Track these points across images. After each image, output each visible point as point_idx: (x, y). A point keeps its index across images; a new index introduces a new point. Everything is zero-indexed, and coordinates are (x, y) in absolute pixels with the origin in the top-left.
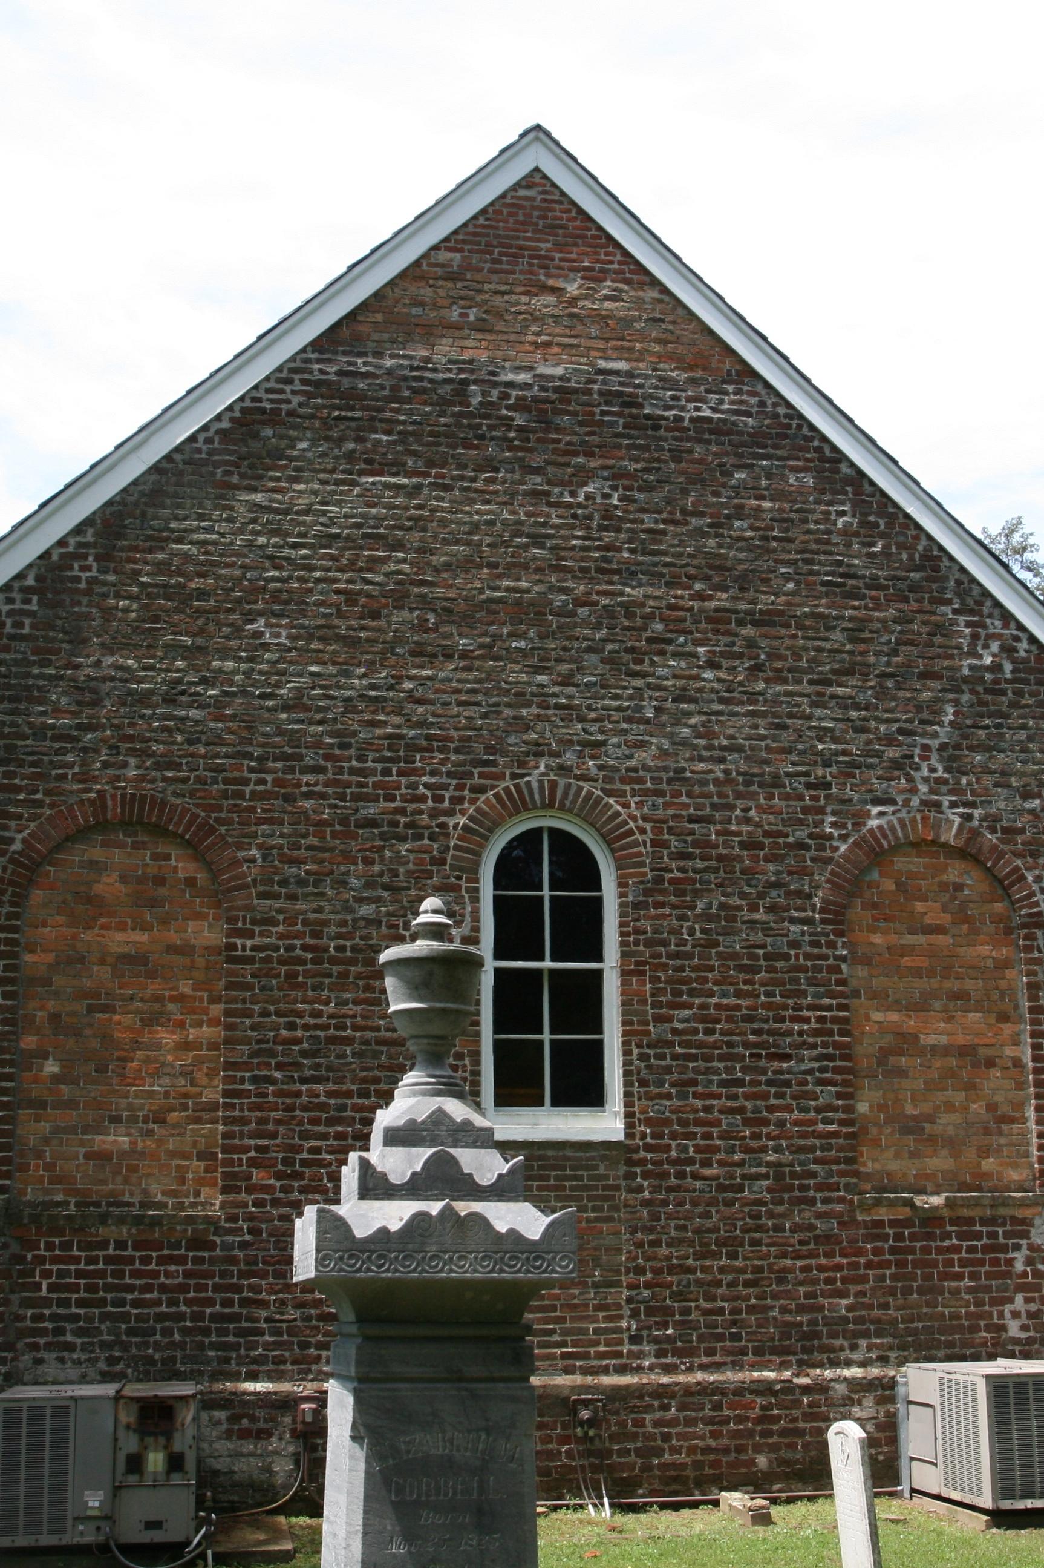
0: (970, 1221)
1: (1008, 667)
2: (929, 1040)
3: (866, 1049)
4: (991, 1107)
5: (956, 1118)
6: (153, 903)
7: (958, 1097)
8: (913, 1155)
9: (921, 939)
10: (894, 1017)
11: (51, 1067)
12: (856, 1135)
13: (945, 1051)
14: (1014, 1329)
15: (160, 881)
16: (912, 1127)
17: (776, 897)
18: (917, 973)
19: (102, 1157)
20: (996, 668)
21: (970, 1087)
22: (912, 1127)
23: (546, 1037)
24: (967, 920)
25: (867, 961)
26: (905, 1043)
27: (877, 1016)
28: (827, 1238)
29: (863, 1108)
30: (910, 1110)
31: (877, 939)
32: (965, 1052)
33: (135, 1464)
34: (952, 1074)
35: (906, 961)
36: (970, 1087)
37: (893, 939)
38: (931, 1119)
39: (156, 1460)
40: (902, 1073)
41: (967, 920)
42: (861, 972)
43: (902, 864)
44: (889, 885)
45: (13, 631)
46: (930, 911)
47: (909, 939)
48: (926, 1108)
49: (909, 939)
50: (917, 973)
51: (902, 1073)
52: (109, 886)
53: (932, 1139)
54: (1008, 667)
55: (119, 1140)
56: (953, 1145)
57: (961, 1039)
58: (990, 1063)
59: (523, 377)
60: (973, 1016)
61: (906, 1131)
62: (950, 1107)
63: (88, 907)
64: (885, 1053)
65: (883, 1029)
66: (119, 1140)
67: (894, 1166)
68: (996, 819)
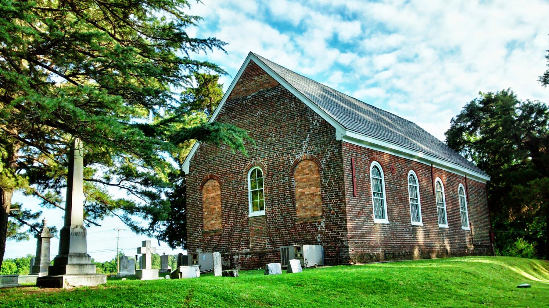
0: (312, 222)
1: (318, 124)
2: (306, 193)
3: (297, 196)
4: (316, 203)
5: (311, 205)
6: (214, 189)
7: (311, 202)
8: (305, 212)
9: (305, 176)
10: (301, 190)
11: (206, 213)
12: (295, 210)
13: (308, 194)
14: (319, 240)
15: (215, 186)
16: (304, 208)
17: (283, 173)
18: (304, 182)
19: (211, 224)
20: (316, 125)
21: (313, 200)
22: (304, 208)
23: (259, 200)
24: (312, 171)
25: (297, 181)
26: (303, 194)
27: (299, 190)
28: (292, 227)
29: (297, 205)
30: (304, 205)
31: (299, 177)
32: (312, 194)
33: (193, 262)
34: (310, 198)
35: (303, 180)
36: (313, 200)
37: (301, 177)
38: (307, 206)
39: (195, 262)
40: (302, 199)
41: (312, 171)
42: (297, 183)
43: (302, 164)
44: (300, 168)
45: (469, 226)
46: (306, 171)
47: (303, 176)
48: (306, 204)
49: (303, 176)
50: (304, 182)
51: (302, 199)
52: (210, 188)
53: (307, 210)
54: (318, 124)
55: (212, 222)
56: (310, 210)
57: (311, 192)
58: (316, 195)
59: (250, 97)
60: (313, 188)
61: (303, 208)
62: (310, 204)
63: (208, 191)
64: (300, 196)
65: (300, 192)
66: (212, 222)
67: (302, 214)
68: (315, 152)
